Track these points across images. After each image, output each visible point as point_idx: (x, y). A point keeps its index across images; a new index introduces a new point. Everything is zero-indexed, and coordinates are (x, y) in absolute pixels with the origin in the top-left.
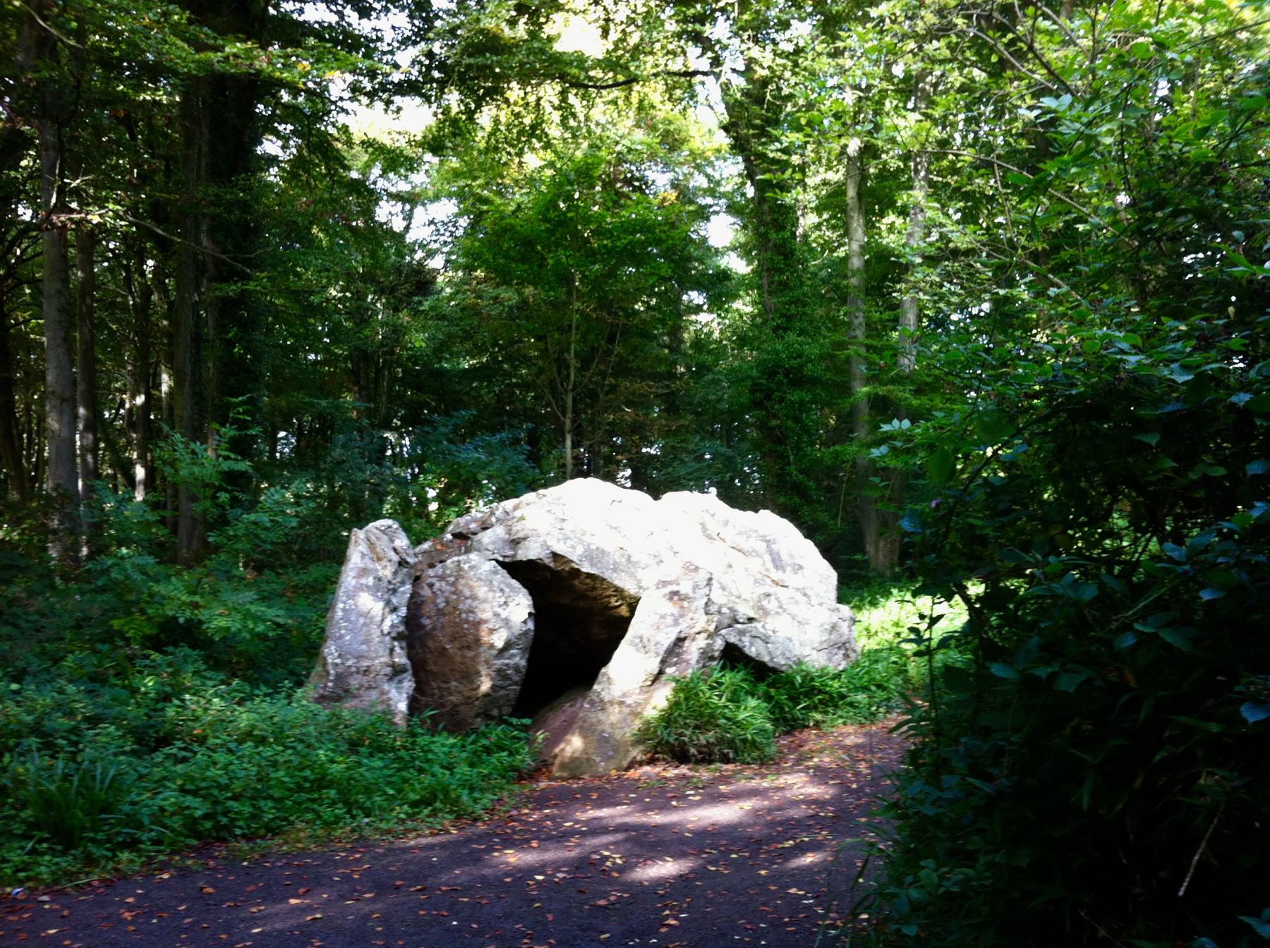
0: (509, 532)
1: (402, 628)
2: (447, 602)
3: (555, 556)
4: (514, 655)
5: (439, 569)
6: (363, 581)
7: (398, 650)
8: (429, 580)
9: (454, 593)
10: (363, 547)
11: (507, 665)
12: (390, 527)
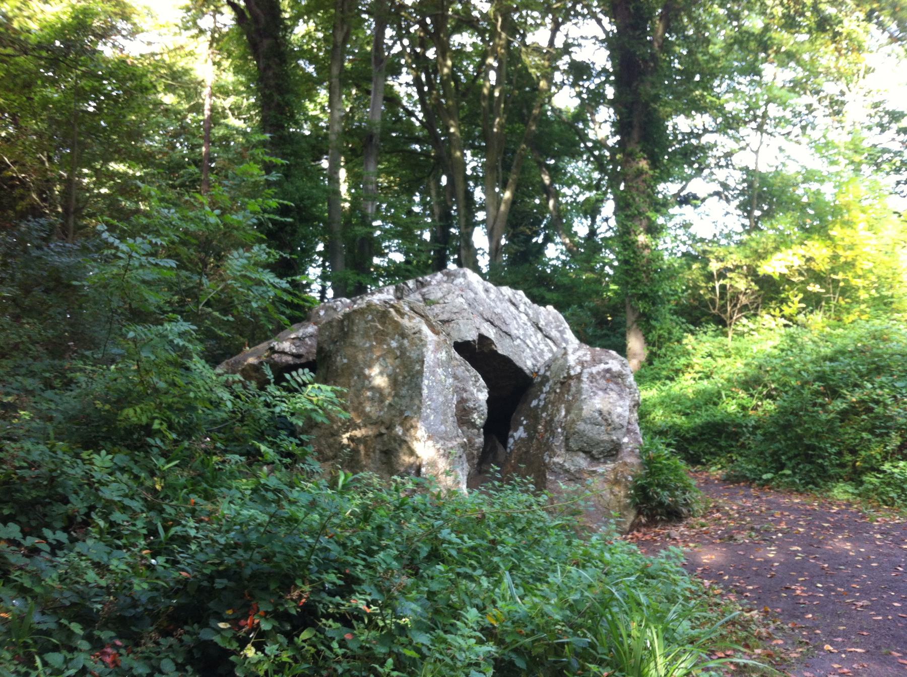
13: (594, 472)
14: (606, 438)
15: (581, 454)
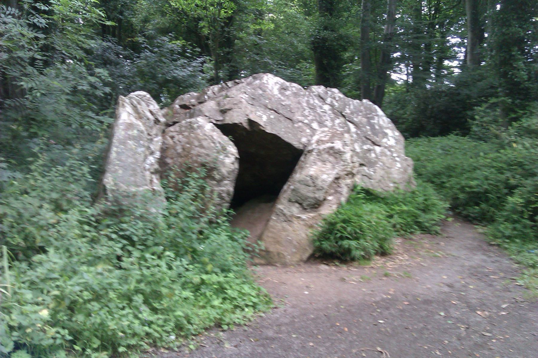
0: (219, 104)
1: (156, 166)
2: (184, 149)
3: (251, 122)
4: (226, 184)
5: (176, 127)
6: (130, 133)
7: (155, 181)
8: (171, 134)
9: (188, 143)
10: (129, 109)
11: (222, 191)
12: (145, 96)
13: (299, 217)
14: (311, 195)
15: (297, 205)
